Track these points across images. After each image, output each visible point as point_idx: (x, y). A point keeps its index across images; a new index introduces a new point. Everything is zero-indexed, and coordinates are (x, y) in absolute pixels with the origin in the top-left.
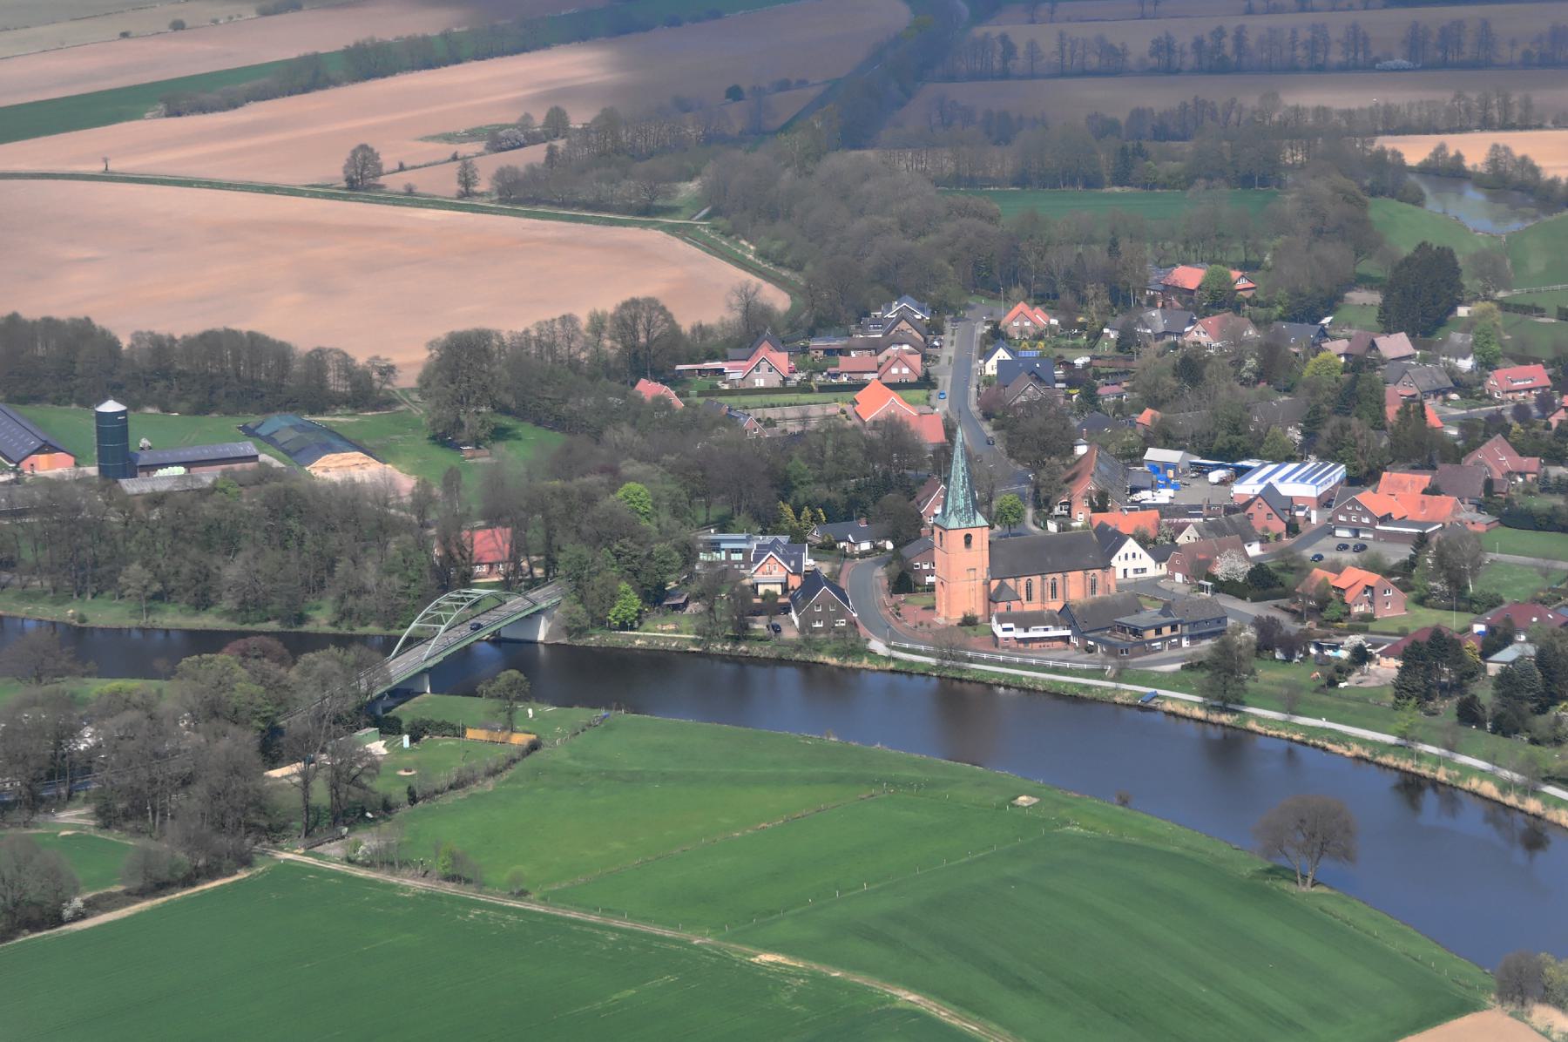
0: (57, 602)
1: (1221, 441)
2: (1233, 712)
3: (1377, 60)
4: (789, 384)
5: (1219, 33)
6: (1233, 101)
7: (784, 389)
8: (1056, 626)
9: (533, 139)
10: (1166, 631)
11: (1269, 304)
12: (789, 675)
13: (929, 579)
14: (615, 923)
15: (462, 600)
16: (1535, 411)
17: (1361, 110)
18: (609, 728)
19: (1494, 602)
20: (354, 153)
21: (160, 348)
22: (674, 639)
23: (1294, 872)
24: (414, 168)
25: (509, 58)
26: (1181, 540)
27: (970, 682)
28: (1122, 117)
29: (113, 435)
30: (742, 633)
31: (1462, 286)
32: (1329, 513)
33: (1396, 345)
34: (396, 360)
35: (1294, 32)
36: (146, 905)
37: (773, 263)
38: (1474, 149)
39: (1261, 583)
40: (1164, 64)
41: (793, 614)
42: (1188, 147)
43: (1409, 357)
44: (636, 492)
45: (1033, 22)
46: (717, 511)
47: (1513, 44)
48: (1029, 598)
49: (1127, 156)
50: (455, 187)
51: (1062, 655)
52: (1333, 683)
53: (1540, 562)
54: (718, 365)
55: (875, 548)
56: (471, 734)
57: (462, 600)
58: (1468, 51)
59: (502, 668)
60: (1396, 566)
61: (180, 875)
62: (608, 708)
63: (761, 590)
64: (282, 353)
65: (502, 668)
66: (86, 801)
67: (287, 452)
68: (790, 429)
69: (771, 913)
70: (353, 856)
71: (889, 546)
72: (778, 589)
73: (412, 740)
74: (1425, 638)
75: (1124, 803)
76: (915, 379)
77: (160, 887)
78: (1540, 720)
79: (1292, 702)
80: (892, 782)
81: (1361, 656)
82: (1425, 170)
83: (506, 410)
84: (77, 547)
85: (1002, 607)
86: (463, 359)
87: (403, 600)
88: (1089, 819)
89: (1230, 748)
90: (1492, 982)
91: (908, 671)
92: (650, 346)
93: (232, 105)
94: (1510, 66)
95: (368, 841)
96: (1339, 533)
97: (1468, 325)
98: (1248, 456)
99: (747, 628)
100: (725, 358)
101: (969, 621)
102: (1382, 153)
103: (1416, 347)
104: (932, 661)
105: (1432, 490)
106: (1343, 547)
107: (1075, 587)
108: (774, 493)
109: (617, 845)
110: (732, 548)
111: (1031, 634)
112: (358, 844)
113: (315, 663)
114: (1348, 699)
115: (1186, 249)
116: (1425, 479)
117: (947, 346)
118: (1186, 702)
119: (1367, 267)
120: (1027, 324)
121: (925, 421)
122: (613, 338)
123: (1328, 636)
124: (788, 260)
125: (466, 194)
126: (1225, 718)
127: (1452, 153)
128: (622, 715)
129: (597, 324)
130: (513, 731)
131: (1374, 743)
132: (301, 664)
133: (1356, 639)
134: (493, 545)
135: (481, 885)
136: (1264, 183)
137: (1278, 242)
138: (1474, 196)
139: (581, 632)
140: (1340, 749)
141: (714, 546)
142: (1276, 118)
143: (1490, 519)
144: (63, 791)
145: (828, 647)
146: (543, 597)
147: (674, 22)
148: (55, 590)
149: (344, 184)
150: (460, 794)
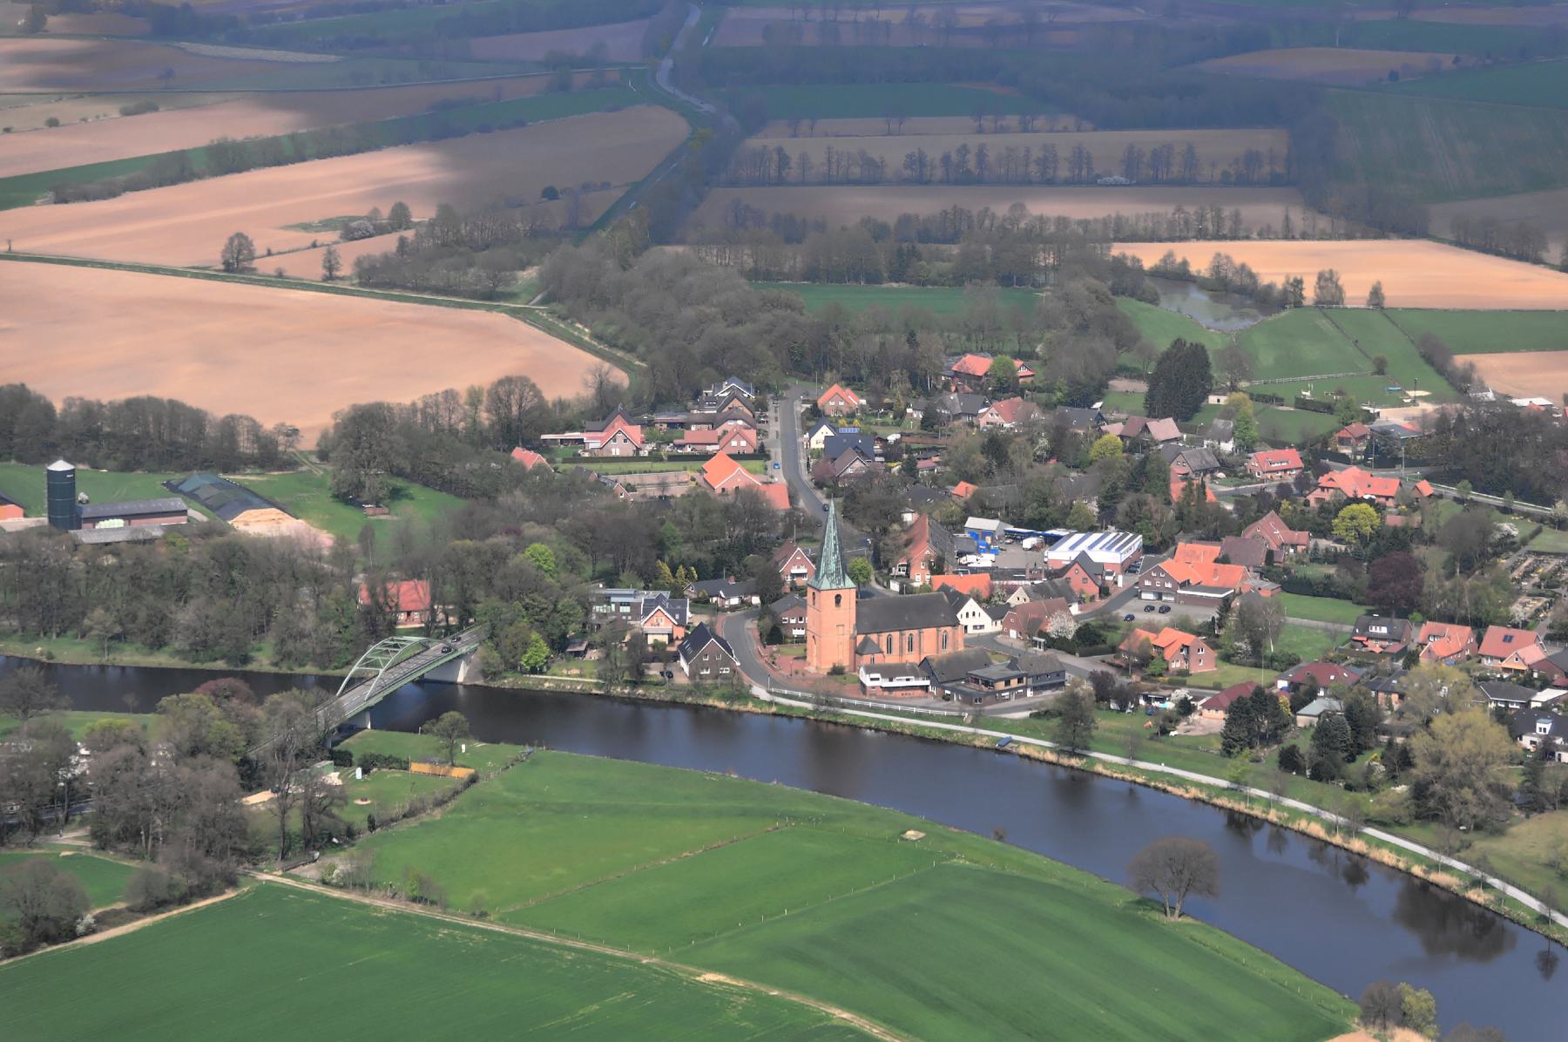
0: (25, 640)
1: (1029, 513)
3: (1098, 176)
4: (642, 453)
5: (964, 150)
6: (987, 209)
7: (637, 458)
8: (917, 677)
9: (381, 230)
10: (1014, 683)
11: (1050, 390)
12: (679, 716)
13: (796, 632)
14: (569, 943)
15: (396, 646)
16: (1295, 491)
17: (1096, 220)
18: (535, 763)
19: (1292, 662)
20: (231, 240)
21: (90, 412)
23: (1163, 905)
25: (335, 159)
26: (1013, 600)
30: (639, 679)
31: (1211, 377)
32: (1136, 578)
33: (1164, 429)
34: (298, 425)
35: (1028, 150)
36: (148, 921)
37: (607, 344)
38: (1199, 257)
39: (1088, 640)
40: (917, 176)
41: (682, 662)
42: (955, 250)
43: (1176, 439)
44: (541, 551)
45: (795, 136)
46: (605, 565)
47: (1213, 165)
48: (890, 651)
49: (899, 256)
50: (319, 272)
51: (922, 702)
53: (1330, 626)
54: (576, 435)
55: (743, 602)
56: (415, 767)
57: (396, 646)
58: (1176, 170)
59: (425, 705)
60: (1200, 627)
61: (177, 894)
62: (531, 745)
63: (650, 640)
64: (197, 419)
65: (425, 705)
66: (82, 824)
67: (209, 507)
68: (651, 494)
69: (707, 935)
70: (327, 879)
71: (756, 600)
72: (665, 639)
73: (365, 772)
74: (1247, 695)
75: (1000, 838)
76: (751, 451)
77: (160, 905)
78: (1352, 767)
79: (1133, 750)
80: (794, 817)
81: (1186, 708)
82: (1156, 273)
83: (399, 473)
84: (40, 590)
85: (866, 659)
86: (365, 432)
87: (336, 644)
88: (972, 852)
89: (1076, 788)
90: (1358, 1009)
91: (786, 715)
92: (519, 421)
93: (111, 193)
94: (1211, 184)
95: (341, 864)
96: (1144, 596)
97: (1227, 413)
98: (1056, 526)
99: (641, 674)
100: (582, 429)
101: (837, 671)
102: (1119, 262)
103: (1181, 430)
104: (809, 706)
105: (1223, 560)
106: (1150, 609)
107: (929, 643)
108: (654, 552)
109: (559, 871)
110: (623, 600)
111: (895, 683)
112: (333, 868)
113: (280, 704)
114: (1180, 746)
115: (969, 339)
116: (1215, 550)
117: (772, 422)
118: (1038, 746)
119: (1125, 358)
121: (775, 489)
122: (488, 411)
123: (1155, 689)
124: (621, 342)
125: (330, 278)
126: (1074, 762)
127: (1179, 260)
128: (541, 752)
129: (474, 397)
130: (453, 765)
131: (1209, 786)
132: (267, 704)
133: (1182, 693)
134: (415, 596)
135: (445, 908)
136: (1020, 282)
137: (1048, 335)
138: (1199, 298)
139: (495, 675)
140: (1180, 791)
141: (607, 600)
142: (1022, 225)
143: (1275, 586)
144: (61, 816)
145: (717, 692)
146: (466, 643)
147: (485, 129)
148: (24, 629)
149: (222, 267)
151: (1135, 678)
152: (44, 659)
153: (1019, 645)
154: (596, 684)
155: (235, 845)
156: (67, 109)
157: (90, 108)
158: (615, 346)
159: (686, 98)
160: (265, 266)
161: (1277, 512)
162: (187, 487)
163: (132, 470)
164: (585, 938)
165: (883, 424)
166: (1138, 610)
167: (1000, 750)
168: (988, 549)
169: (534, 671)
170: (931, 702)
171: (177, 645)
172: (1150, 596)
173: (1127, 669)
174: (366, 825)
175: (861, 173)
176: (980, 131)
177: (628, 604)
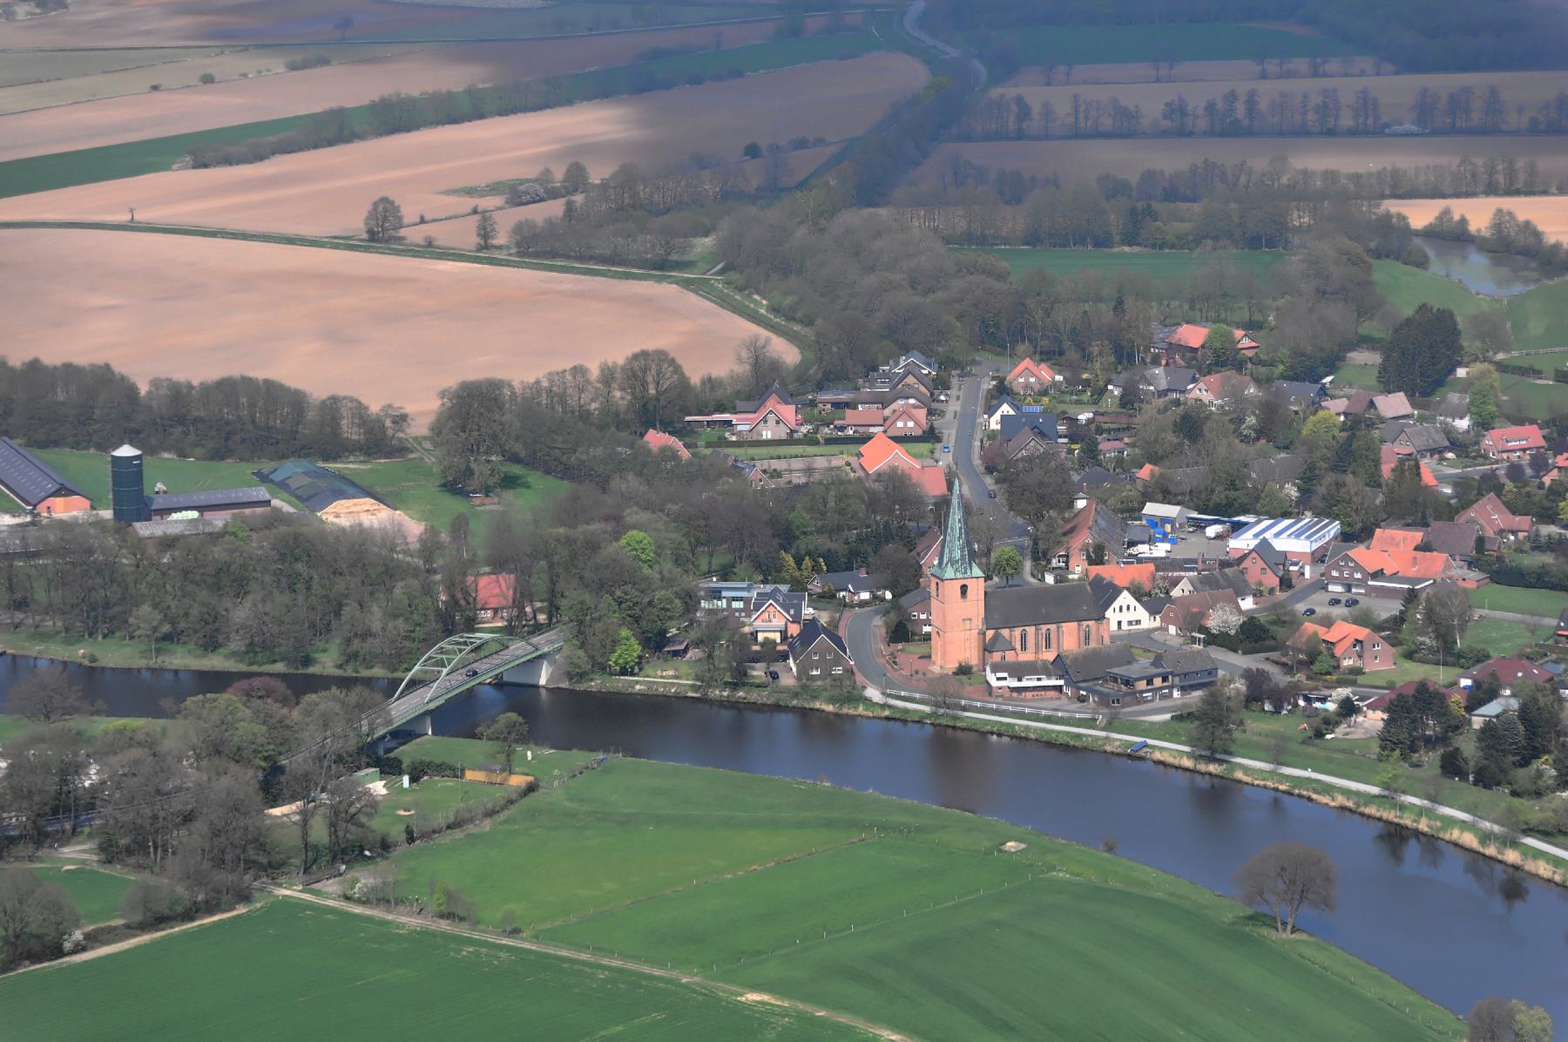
0: (69, 642)
1: (1219, 496)
2: (1221, 762)
3: (1387, 125)
5: (1232, 97)
6: (1243, 163)
8: (1049, 676)
9: (553, 194)
10: (1158, 682)
12: (785, 721)
14: (605, 961)
15: (465, 643)
16: (1529, 471)
17: (1370, 175)
19: (1481, 657)
20: (376, 205)
21: (178, 395)
22: (673, 684)
23: (1275, 919)
24: (435, 220)
27: (963, 729)
28: (1134, 179)
29: (128, 480)
30: (740, 679)
31: (1462, 348)
32: (1322, 568)
33: (1394, 404)
34: (409, 409)
35: (1305, 97)
36: (145, 938)
37: (784, 318)
38: (1478, 214)
39: (1252, 636)
40: (1177, 127)
42: (1197, 208)
44: (640, 540)
45: (1048, 84)
47: (1520, 111)
48: (1024, 647)
49: (1137, 217)
51: (1055, 704)
52: (1319, 735)
53: (1528, 618)
54: (726, 416)
55: (875, 597)
59: (519, 710)
60: (1386, 621)
61: (179, 909)
62: (606, 751)
64: (297, 400)
65: (519, 710)
66: (90, 836)
69: (759, 953)
70: (350, 893)
71: (889, 595)
72: (777, 637)
74: (1411, 691)
75: (1110, 849)
76: (919, 432)
77: (160, 921)
79: (1278, 753)
80: (883, 827)
82: (1430, 233)
83: (515, 459)
84: (88, 587)
85: (997, 657)
86: (474, 408)
88: (1075, 864)
89: (1217, 797)
91: (901, 719)
92: (661, 396)
94: (1517, 132)
95: (365, 879)
96: (1331, 588)
97: (1465, 386)
98: (1245, 512)
100: (734, 411)
101: (964, 670)
103: (1414, 406)
104: (927, 709)
105: (1424, 547)
107: (1069, 637)
110: (733, 596)
111: (1025, 683)
115: (1192, 308)
116: (1418, 536)
117: (953, 401)
120: (1032, 380)
121: (927, 473)
122: (622, 389)
123: (1316, 689)
124: (799, 315)
125: (485, 247)
126: (1212, 768)
127: (1457, 217)
129: (608, 376)
131: (1358, 793)
133: (1343, 692)
135: (475, 923)
136: (1271, 244)
137: (1281, 302)
139: (582, 676)
142: (1284, 180)
144: (68, 826)
147: (696, 81)
149: (365, 236)
150: (458, 834)
151: (1300, 677)
152: (86, 663)
153: (1178, 641)
154: (692, 686)
155: (264, 858)
156: (227, 64)
157: (251, 63)
158: (793, 319)
159: (931, 42)
160: (415, 235)
161: (1499, 495)
162: (277, 477)
163: (223, 459)
164: (622, 956)
165: (1078, 402)
166: (1321, 604)
167: (1134, 756)
168: (1164, 539)
169: (624, 672)
170: (1065, 706)
171: (233, 646)
172: (1338, 589)
173: (1291, 668)
174: (404, 836)
175: (1109, 119)
176: (1264, 76)
177: (741, 599)
